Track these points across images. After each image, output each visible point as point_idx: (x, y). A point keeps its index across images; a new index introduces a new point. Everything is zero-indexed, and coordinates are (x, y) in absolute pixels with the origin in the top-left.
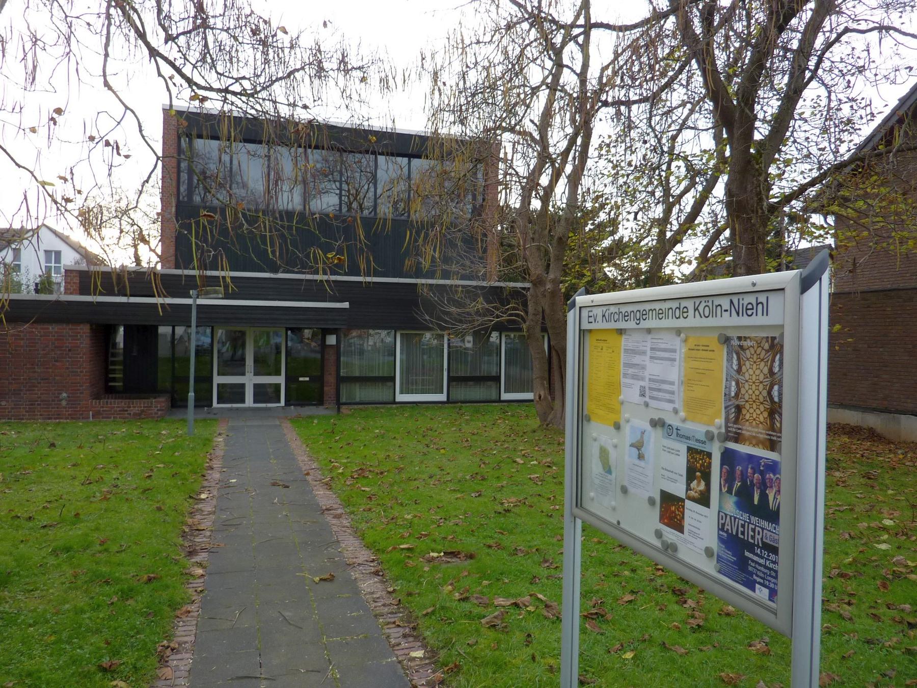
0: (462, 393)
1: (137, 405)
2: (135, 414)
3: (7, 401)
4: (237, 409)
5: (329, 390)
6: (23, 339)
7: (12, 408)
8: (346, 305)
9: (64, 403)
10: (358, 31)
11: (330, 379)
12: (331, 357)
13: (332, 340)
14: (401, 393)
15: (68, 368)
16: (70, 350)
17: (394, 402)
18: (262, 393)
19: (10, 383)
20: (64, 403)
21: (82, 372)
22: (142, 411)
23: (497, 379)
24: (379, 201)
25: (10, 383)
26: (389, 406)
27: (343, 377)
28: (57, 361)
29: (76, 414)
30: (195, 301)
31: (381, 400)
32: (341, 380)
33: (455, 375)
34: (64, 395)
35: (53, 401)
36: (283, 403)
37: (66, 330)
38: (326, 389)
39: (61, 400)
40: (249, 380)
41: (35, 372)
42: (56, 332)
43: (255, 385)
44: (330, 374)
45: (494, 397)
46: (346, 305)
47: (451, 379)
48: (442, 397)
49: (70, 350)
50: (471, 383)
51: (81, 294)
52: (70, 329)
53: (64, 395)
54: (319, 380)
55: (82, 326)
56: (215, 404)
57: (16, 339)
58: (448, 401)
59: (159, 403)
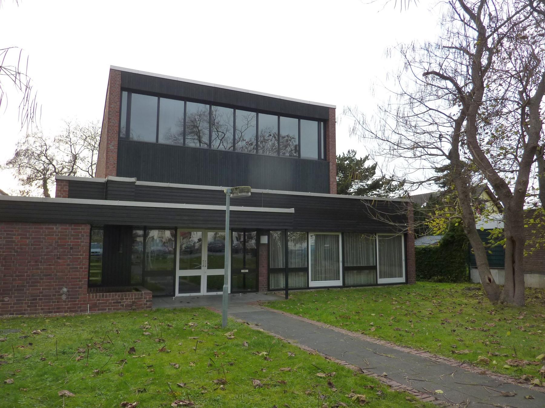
0: (352, 279)
1: (130, 297)
2: (127, 306)
3: (10, 297)
4: (193, 298)
5: (262, 279)
6: (28, 238)
7: (15, 304)
8: (292, 210)
9: (64, 297)
11: (263, 270)
12: (263, 253)
13: (264, 240)
14: (381, 277)
15: (68, 265)
16: (71, 248)
17: (308, 288)
18: (215, 283)
20: (64, 297)
21: (81, 268)
22: (134, 302)
23: (305, 270)
24: (429, 153)
26: (304, 291)
27: (272, 269)
28: (58, 258)
29: (75, 308)
30: (228, 208)
31: (297, 286)
32: (272, 271)
33: (349, 265)
35: (54, 295)
37: (69, 229)
38: (260, 278)
39: (62, 294)
40: (204, 273)
44: (263, 267)
45: (372, 281)
46: (292, 210)
47: (345, 269)
48: (339, 283)
49: (71, 248)
50: (355, 272)
51: (69, 197)
52: (72, 229)
53: (65, 290)
54: (255, 271)
55: (83, 226)
56: (177, 294)
57: (21, 238)
58: (344, 286)
59: (146, 294)
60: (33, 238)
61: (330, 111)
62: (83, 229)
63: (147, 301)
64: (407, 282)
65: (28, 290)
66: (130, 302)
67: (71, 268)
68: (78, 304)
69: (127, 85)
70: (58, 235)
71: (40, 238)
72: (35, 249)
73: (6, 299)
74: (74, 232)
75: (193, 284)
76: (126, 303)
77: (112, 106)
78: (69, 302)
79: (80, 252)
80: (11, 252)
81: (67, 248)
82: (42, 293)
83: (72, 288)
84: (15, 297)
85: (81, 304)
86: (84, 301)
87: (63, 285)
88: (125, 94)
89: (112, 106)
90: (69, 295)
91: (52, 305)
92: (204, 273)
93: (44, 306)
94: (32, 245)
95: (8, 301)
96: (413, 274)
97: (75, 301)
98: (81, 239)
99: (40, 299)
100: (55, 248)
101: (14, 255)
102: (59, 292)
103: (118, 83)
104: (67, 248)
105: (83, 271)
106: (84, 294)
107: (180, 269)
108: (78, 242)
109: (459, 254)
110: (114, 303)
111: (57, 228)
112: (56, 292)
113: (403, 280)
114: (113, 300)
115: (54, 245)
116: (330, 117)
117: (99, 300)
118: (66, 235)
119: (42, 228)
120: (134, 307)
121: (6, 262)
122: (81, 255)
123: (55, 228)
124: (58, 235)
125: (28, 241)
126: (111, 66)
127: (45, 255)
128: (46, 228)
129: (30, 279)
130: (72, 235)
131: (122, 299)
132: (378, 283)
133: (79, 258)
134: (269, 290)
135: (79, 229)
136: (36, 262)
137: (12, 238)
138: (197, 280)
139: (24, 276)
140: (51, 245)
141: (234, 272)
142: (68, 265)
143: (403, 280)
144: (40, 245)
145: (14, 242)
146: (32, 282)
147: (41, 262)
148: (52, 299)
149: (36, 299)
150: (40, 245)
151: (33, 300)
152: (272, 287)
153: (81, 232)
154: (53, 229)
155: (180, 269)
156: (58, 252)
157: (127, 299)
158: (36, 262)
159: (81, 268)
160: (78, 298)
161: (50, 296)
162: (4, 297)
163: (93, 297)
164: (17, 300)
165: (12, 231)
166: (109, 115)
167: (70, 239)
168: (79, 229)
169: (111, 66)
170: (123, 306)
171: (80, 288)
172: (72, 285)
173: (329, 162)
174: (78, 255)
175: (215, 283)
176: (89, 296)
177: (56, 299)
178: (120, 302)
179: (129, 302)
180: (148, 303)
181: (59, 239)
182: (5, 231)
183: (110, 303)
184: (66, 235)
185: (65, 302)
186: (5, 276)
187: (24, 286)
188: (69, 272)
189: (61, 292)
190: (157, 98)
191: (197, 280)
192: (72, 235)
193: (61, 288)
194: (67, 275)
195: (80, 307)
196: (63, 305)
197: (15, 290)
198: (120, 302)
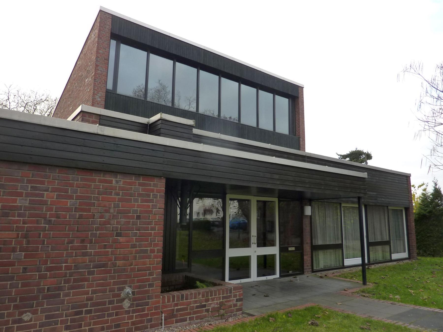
3: (35, 312)
6: (71, 197)
9: (126, 304)
10: (41, 93)
11: (307, 248)
15: (134, 246)
16: (138, 217)
17: (344, 267)
18: (265, 264)
19: (41, 277)
20: (126, 304)
21: (152, 251)
22: (221, 304)
25: (41, 277)
28: (119, 235)
32: (315, 248)
34: (128, 290)
35: (111, 302)
36: (278, 275)
37: (136, 185)
39: (123, 300)
41: (85, 254)
42: (122, 189)
43: (258, 256)
44: (307, 243)
49: (138, 217)
52: (140, 185)
53: (128, 290)
57: (59, 197)
60: (78, 198)
61: (300, 89)
62: (155, 185)
63: (237, 300)
64: (409, 258)
65: (67, 295)
66: (217, 304)
67: (137, 252)
68: (147, 315)
69: (116, 32)
70: (119, 195)
71: (89, 198)
72: (81, 217)
73: (26, 317)
74: (143, 190)
75: (241, 267)
76: (213, 306)
77: (101, 51)
78: (134, 311)
79: (150, 223)
80: (38, 222)
81: (132, 217)
82: (91, 299)
83: (139, 287)
84: (43, 311)
85: (152, 314)
86: (156, 308)
87: (125, 283)
88: (113, 43)
89: (101, 51)
90: (134, 300)
91: (107, 322)
92: (254, 252)
93: (95, 324)
94: (76, 210)
95: (31, 320)
96: (415, 251)
97: (143, 310)
98: (152, 201)
99: (89, 312)
100: (114, 217)
101: (44, 229)
102: (119, 295)
103: (108, 27)
104: (132, 217)
105: (156, 257)
106: (157, 297)
107: (231, 247)
108: (149, 206)
109: (437, 229)
110: (197, 307)
111: (117, 182)
112: (114, 296)
113: (405, 255)
114: (195, 302)
115: (112, 211)
116: (300, 95)
117: (176, 305)
118: (131, 195)
119: (94, 181)
120: (222, 312)
121: (28, 242)
122: (153, 229)
123: (114, 180)
124: (119, 195)
125: (69, 202)
126: (101, 7)
127: (97, 229)
128: (100, 181)
129: (71, 275)
130: (140, 195)
131: (207, 300)
132: (393, 258)
133: (150, 235)
134: (313, 271)
135: (150, 185)
136: (83, 241)
137: (42, 195)
138: (246, 260)
139: (61, 268)
140: (107, 211)
141: (282, 250)
142: (134, 246)
143: (405, 255)
144: (89, 210)
145: (45, 203)
146: (75, 281)
147: (91, 242)
148: (108, 309)
149: (81, 313)
150: (89, 210)
151: (77, 313)
152: (315, 268)
153: (153, 191)
154: (111, 182)
155: (231, 247)
156: (118, 223)
157: (213, 300)
158: (83, 241)
159: (152, 251)
160: (147, 304)
161: (104, 303)
162: (21, 314)
163: (169, 301)
164: (47, 317)
165: (43, 183)
166: (97, 61)
167: (136, 201)
168: (150, 185)
169: (101, 7)
170: (207, 311)
171: (151, 285)
172: (139, 281)
173: (299, 138)
174: (147, 229)
175: (265, 264)
176: (164, 297)
177: (113, 308)
178: (205, 306)
179: (213, 304)
180: (239, 303)
181: (120, 200)
182: (29, 182)
183: (192, 308)
184: (131, 195)
185: (128, 312)
186: (25, 270)
187: (60, 289)
188: (135, 258)
189: (122, 295)
190: (146, 53)
191: (246, 260)
192: (140, 195)
193: (122, 289)
194: (131, 264)
195: (150, 320)
196: (124, 319)
197: (45, 297)
198: (205, 306)
